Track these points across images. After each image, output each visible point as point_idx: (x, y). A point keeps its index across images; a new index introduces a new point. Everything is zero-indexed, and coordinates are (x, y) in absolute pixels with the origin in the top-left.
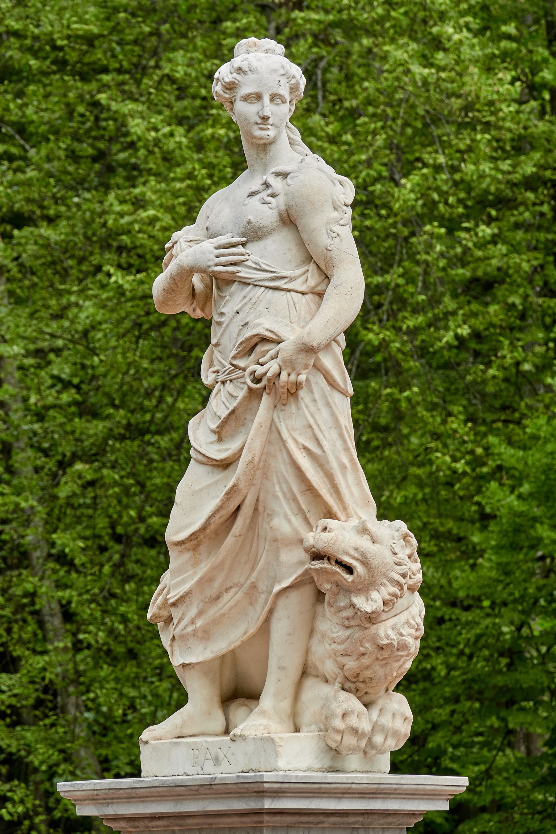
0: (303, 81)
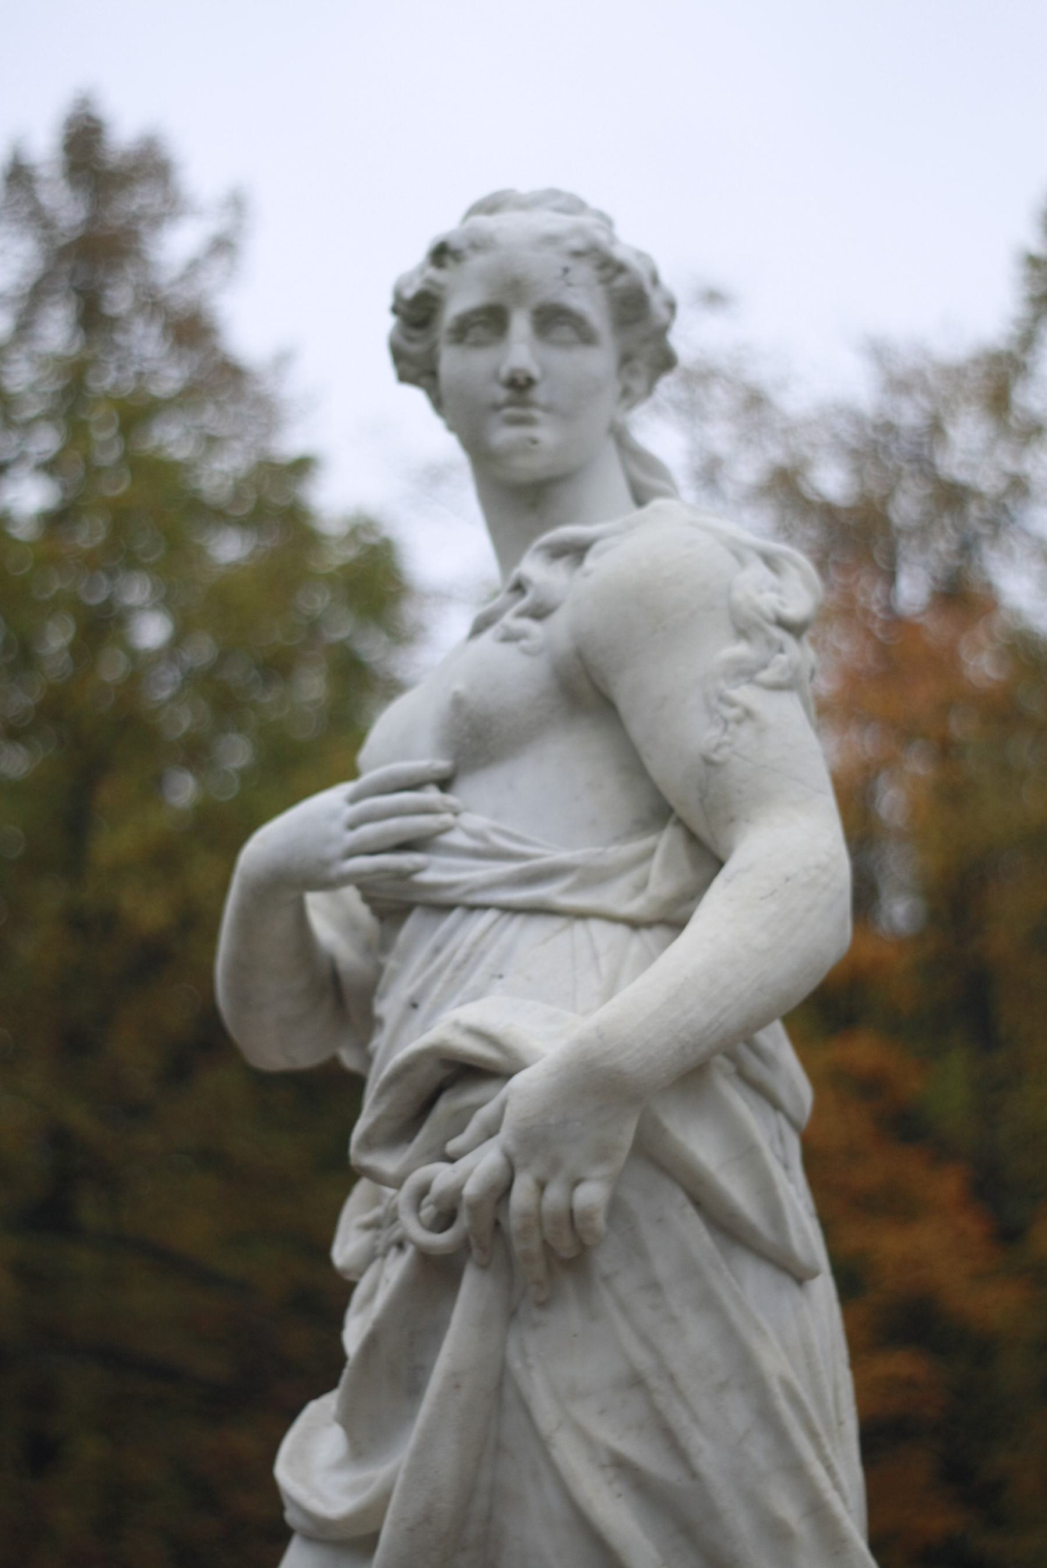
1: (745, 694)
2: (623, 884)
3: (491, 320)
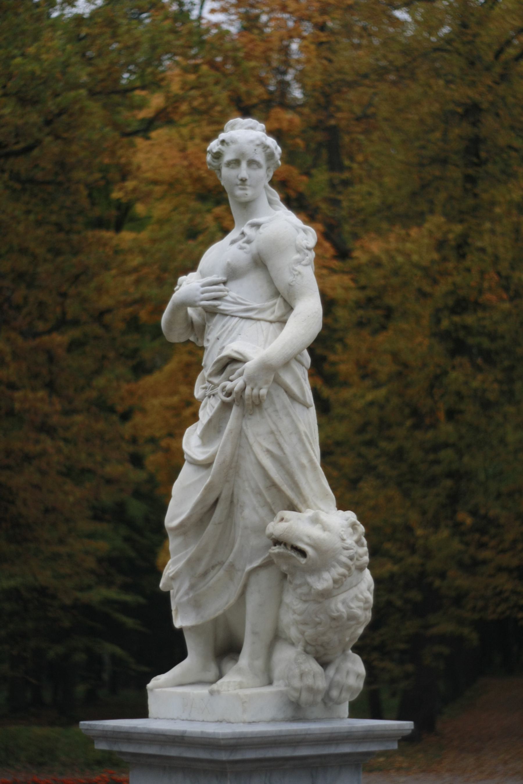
0: (278, 150)
1: (299, 268)
2: (269, 312)
3: (236, 163)
